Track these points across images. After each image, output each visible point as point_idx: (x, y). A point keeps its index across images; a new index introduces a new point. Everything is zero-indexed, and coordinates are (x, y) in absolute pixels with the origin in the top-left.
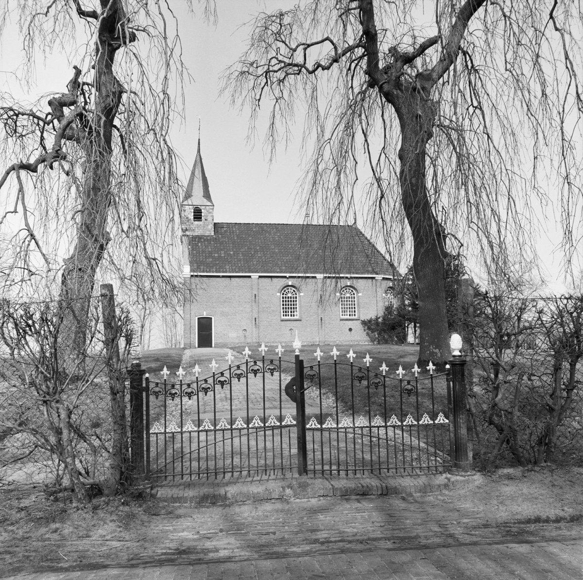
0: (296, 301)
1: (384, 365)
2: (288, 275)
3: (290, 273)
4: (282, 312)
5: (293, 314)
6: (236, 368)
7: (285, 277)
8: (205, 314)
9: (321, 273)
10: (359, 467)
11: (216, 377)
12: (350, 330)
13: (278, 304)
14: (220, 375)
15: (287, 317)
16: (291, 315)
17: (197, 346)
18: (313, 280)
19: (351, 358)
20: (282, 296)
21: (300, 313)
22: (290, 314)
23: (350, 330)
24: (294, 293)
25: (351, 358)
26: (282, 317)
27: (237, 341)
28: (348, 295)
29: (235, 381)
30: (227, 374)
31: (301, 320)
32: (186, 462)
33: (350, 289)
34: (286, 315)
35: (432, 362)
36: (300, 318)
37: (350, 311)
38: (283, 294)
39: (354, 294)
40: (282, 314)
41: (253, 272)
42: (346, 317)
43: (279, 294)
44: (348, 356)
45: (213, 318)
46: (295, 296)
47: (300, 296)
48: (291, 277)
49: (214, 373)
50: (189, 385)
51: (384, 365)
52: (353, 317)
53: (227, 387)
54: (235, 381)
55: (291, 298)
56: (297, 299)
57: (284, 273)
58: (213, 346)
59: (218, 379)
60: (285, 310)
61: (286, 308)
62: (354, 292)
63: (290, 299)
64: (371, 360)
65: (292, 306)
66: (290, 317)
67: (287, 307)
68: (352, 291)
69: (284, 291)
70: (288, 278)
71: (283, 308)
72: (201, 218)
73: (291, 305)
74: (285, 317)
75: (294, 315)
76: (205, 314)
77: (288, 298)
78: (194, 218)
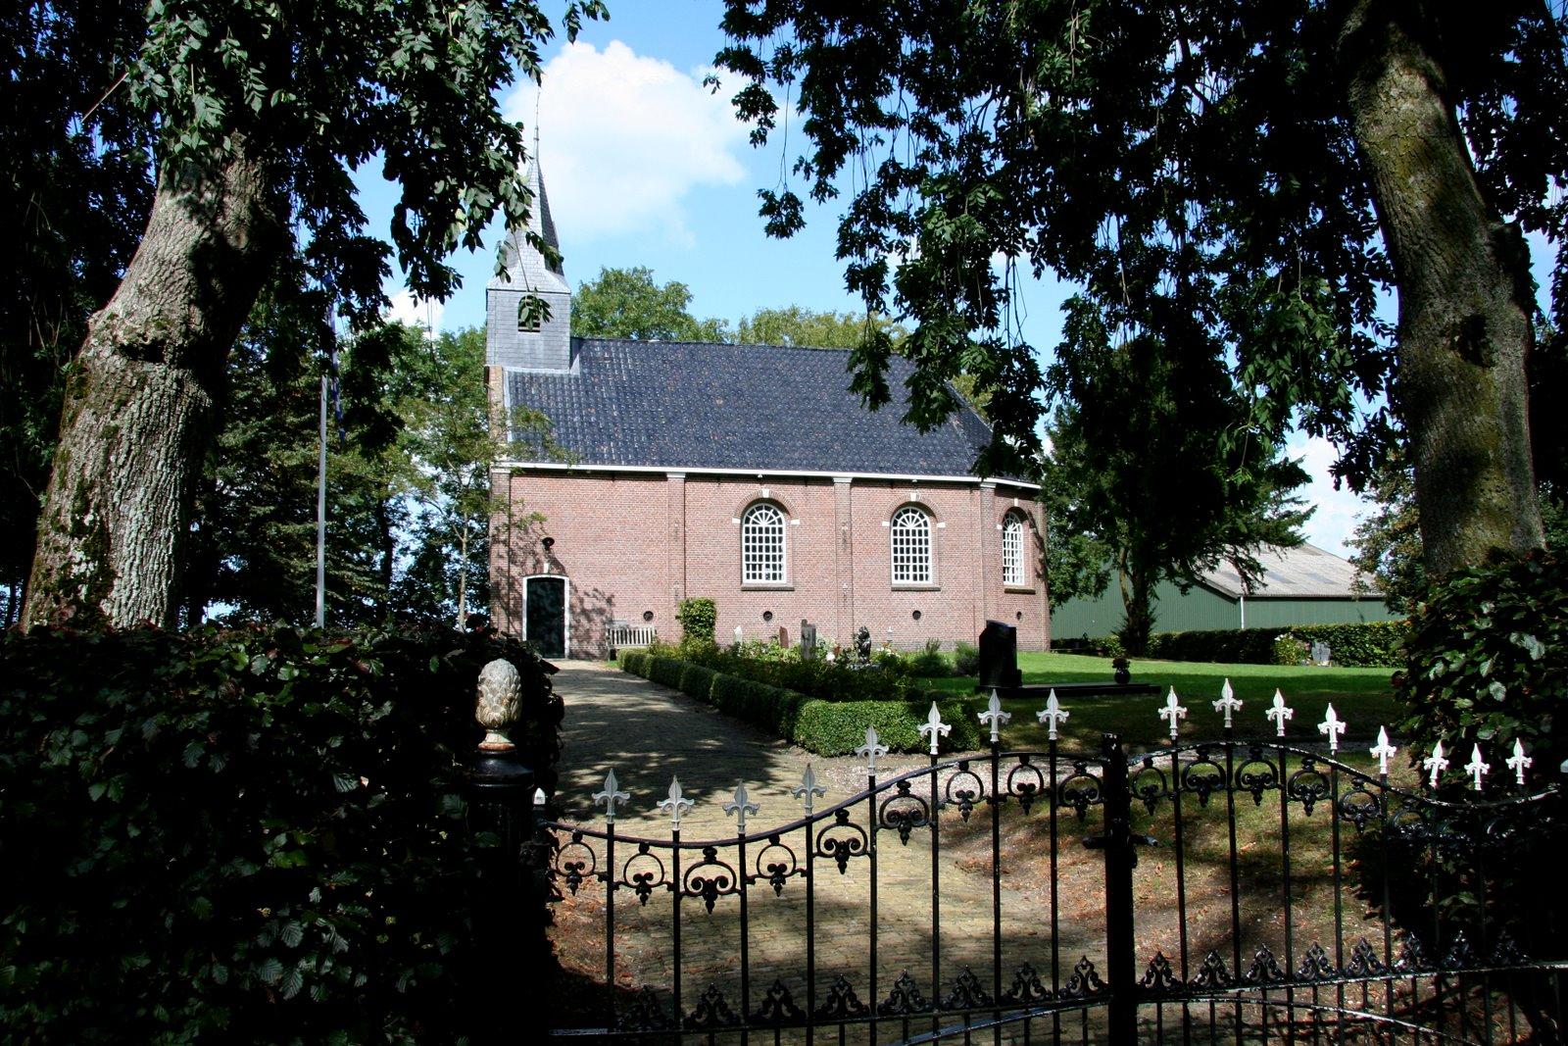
0: (780, 540)
2: (760, 473)
3: (767, 467)
5: (918, 573)
6: (894, 790)
7: (753, 479)
9: (844, 469)
11: (881, 797)
12: (917, 615)
15: (757, 581)
16: (915, 578)
19: (1520, 770)
21: (793, 572)
22: (911, 573)
23: (917, 615)
25: (1520, 770)
26: (894, 581)
27: (753, 655)
30: (859, 813)
31: (792, 590)
34: (902, 577)
35: (1389, 731)
36: (791, 585)
37: (915, 568)
40: (745, 572)
41: (670, 464)
42: (905, 583)
47: (788, 526)
50: (710, 854)
52: (923, 584)
54: (887, 841)
56: (784, 535)
57: (751, 467)
59: (828, 835)
60: (751, 562)
61: (902, 559)
62: (927, 518)
63: (764, 535)
65: (918, 555)
67: (905, 555)
71: (896, 559)
73: (914, 551)
74: (751, 580)
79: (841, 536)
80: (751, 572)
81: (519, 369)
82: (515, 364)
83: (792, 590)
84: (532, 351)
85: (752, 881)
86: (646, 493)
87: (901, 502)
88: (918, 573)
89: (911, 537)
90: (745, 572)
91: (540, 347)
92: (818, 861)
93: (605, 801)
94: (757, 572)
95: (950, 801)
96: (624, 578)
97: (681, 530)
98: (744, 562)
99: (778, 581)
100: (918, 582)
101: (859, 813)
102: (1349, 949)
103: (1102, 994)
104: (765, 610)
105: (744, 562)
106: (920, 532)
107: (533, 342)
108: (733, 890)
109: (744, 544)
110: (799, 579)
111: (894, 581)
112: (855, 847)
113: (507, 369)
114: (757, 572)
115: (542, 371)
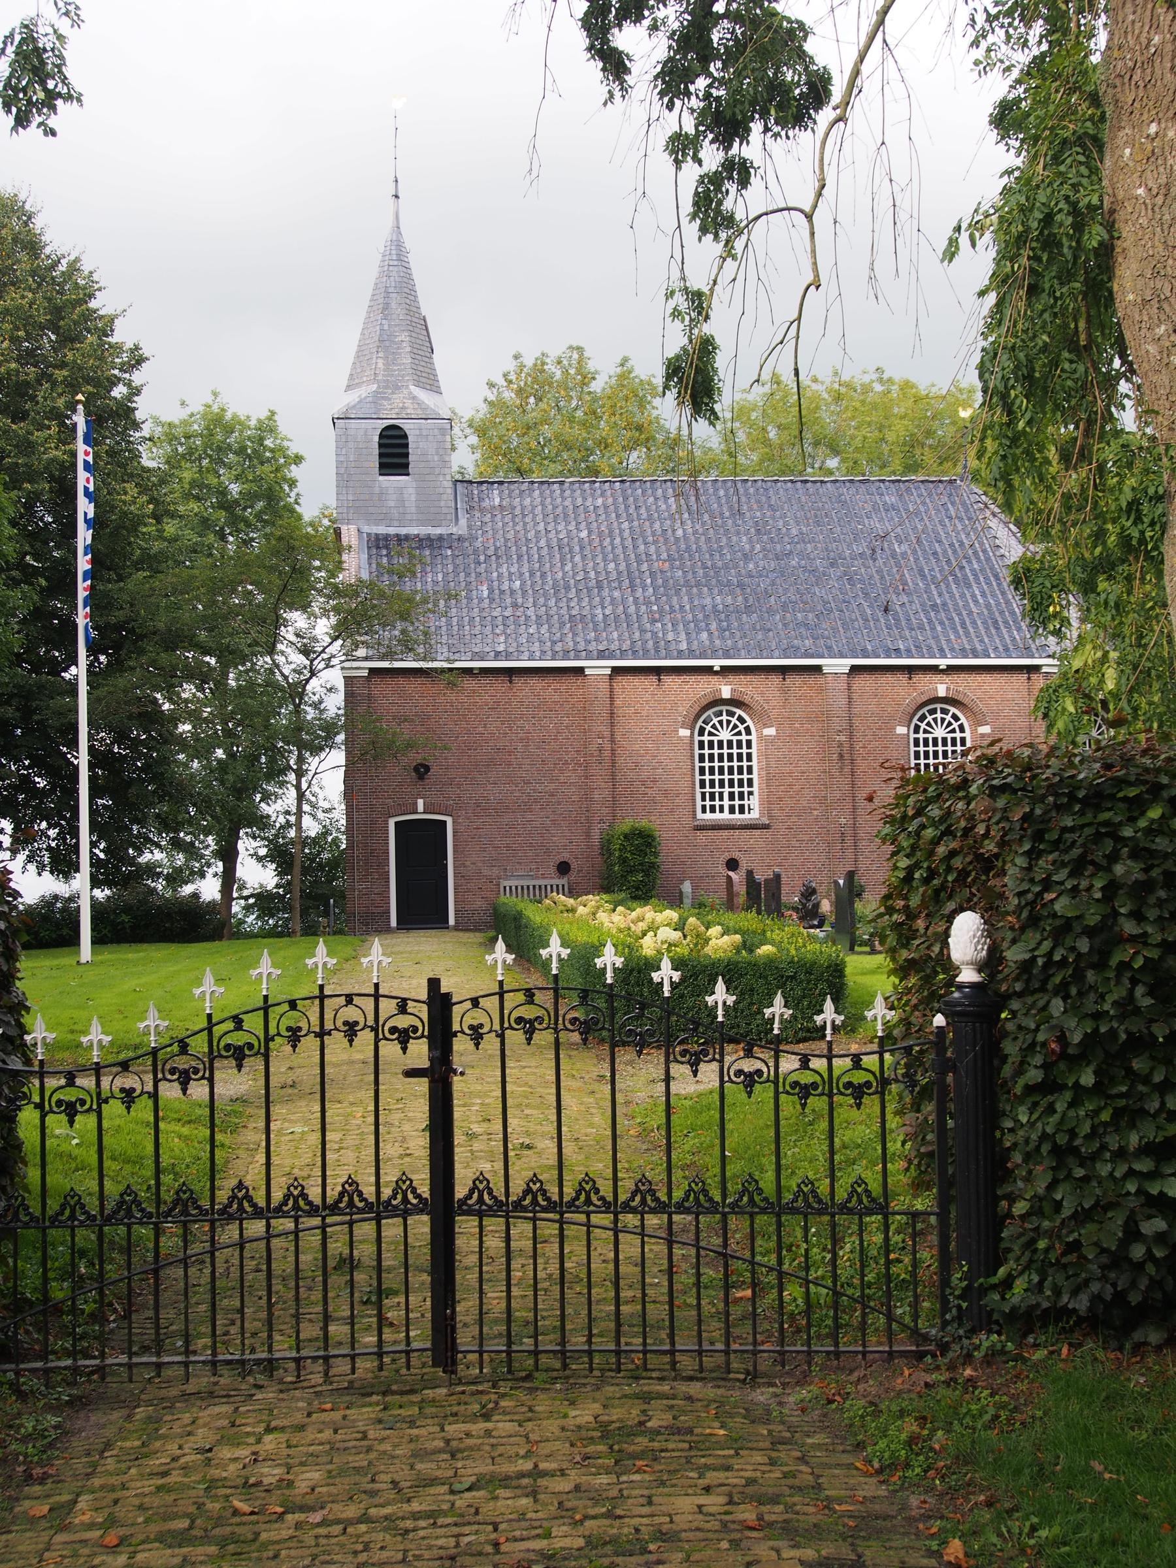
1: (720, 986)
3: (727, 656)
4: (698, 797)
5: (737, 803)
7: (708, 670)
8: (421, 808)
10: (712, 1343)
11: (218, 1030)
13: (686, 766)
14: (230, 1025)
15: (717, 816)
17: (394, 923)
18: (811, 680)
20: (912, 736)
22: (726, 803)
24: (741, 727)
28: (725, 735)
29: (280, 1047)
30: (253, 1023)
32: (633, 1300)
33: (731, 714)
37: (732, 796)
38: (702, 732)
39: (748, 731)
40: (699, 803)
43: (685, 733)
44: (599, 962)
45: (449, 820)
46: (958, 735)
47: (761, 737)
48: (726, 670)
49: (209, 1016)
51: (720, 986)
53: (254, 1064)
55: (730, 746)
58: (452, 921)
64: (676, 976)
66: (726, 815)
68: (741, 720)
69: (706, 722)
70: (716, 673)
72: (406, 466)
74: (709, 816)
75: (742, 811)
76: (421, 808)
77: (720, 743)
78: (382, 466)
79: (836, 750)
80: (708, 803)
81: (382, 530)
82: (377, 522)
83: (766, 827)
84: (401, 501)
85: (106, 1101)
86: (556, 698)
87: (924, 698)
88: (737, 803)
89: (725, 751)
90: (699, 803)
91: (411, 494)
92: (163, 1086)
93: (91, 1041)
94: (717, 803)
95: (279, 1034)
96: (529, 816)
97: (607, 746)
98: (698, 790)
99: (746, 816)
100: (737, 816)
101: (199, 1045)
102: (733, 1187)
103: (422, 1207)
104: (727, 856)
105: (698, 790)
106: (954, 740)
107: (400, 490)
108: (90, 1110)
109: (697, 764)
110: (776, 813)
111: (700, 815)
112: (196, 1073)
113: (366, 529)
114: (717, 803)
115: (414, 531)
